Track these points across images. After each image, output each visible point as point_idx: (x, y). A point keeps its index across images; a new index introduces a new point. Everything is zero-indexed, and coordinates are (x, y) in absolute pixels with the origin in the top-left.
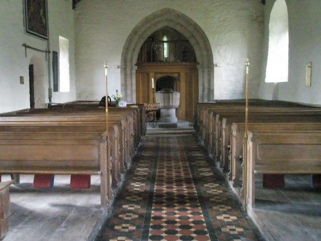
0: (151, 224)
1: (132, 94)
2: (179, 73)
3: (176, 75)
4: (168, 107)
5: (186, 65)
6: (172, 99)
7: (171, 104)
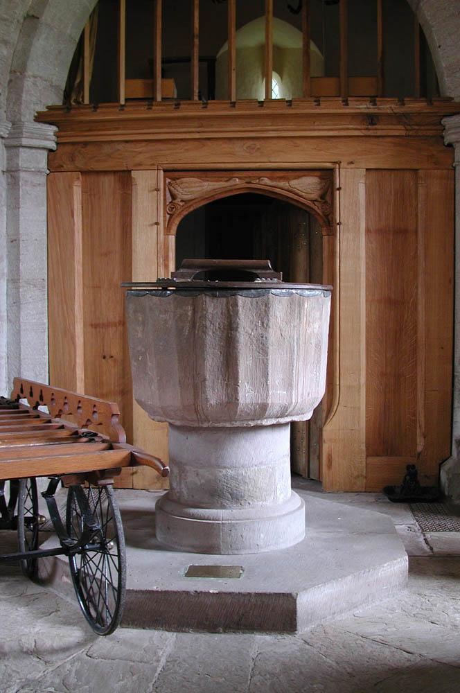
2: (327, 176)
3: (306, 187)
5: (371, 119)
7: (246, 395)
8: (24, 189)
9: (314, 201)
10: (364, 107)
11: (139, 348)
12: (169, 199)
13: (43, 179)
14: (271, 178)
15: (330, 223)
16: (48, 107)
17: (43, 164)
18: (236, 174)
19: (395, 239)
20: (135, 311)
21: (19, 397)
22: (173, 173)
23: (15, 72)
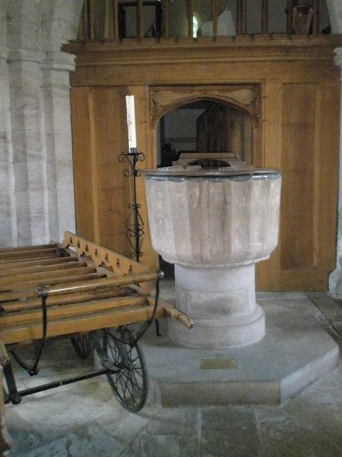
0: (180, 437)
1: (54, 177)
2: (255, 86)
3: (242, 97)
4: (222, 263)
5: (287, 49)
6: (246, 215)
7: (236, 246)
8: (55, 100)
9: (247, 105)
10: (284, 41)
11: (159, 216)
12: (153, 105)
13: (67, 93)
14: (219, 90)
15: (257, 119)
16: (69, 41)
17: (67, 82)
18: (196, 88)
19: (300, 129)
20: (156, 191)
21: (69, 245)
22: (156, 86)
23: (45, 15)
